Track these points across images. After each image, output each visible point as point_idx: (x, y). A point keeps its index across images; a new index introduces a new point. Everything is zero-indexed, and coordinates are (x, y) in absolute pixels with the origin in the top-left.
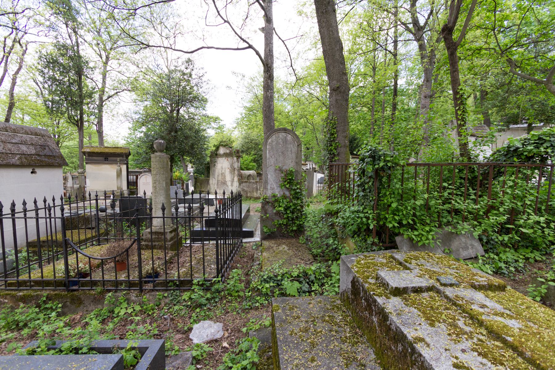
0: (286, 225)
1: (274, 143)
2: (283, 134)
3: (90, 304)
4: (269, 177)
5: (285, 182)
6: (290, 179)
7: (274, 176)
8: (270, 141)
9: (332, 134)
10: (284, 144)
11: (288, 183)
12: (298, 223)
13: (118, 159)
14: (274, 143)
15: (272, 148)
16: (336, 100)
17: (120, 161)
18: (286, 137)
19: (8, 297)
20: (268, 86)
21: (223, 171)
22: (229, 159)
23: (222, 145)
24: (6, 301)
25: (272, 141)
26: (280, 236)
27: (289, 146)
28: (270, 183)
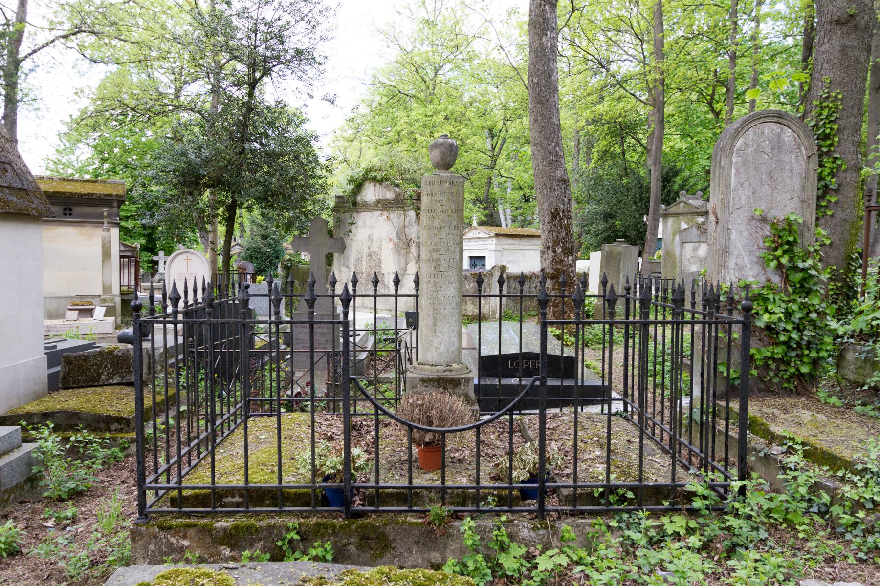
0: (784, 361)
1: (750, 150)
2: (775, 126)
3: (410, 550)
4: (734, 236)
5: (776, 249)
6: (788, 242)
7: (746, 234)
8: (739, 143)
9: (826, 137)
10: (776, 152)
11: (785, 252)
12: (814, 354)
13: (105, 211)
14: (750, 150)
15: (744, 162)
16: (844, 50)
17: (109, 216)
18: (779, 136)
19: (191, 532)
20: (546, 21)
21: (374, 248)
22: (394, 215)
23: (374, 179)
24: (186, 543)
25: (746, 145)
26: (760, 390)
27: (787, 159)
28: (736, 253)
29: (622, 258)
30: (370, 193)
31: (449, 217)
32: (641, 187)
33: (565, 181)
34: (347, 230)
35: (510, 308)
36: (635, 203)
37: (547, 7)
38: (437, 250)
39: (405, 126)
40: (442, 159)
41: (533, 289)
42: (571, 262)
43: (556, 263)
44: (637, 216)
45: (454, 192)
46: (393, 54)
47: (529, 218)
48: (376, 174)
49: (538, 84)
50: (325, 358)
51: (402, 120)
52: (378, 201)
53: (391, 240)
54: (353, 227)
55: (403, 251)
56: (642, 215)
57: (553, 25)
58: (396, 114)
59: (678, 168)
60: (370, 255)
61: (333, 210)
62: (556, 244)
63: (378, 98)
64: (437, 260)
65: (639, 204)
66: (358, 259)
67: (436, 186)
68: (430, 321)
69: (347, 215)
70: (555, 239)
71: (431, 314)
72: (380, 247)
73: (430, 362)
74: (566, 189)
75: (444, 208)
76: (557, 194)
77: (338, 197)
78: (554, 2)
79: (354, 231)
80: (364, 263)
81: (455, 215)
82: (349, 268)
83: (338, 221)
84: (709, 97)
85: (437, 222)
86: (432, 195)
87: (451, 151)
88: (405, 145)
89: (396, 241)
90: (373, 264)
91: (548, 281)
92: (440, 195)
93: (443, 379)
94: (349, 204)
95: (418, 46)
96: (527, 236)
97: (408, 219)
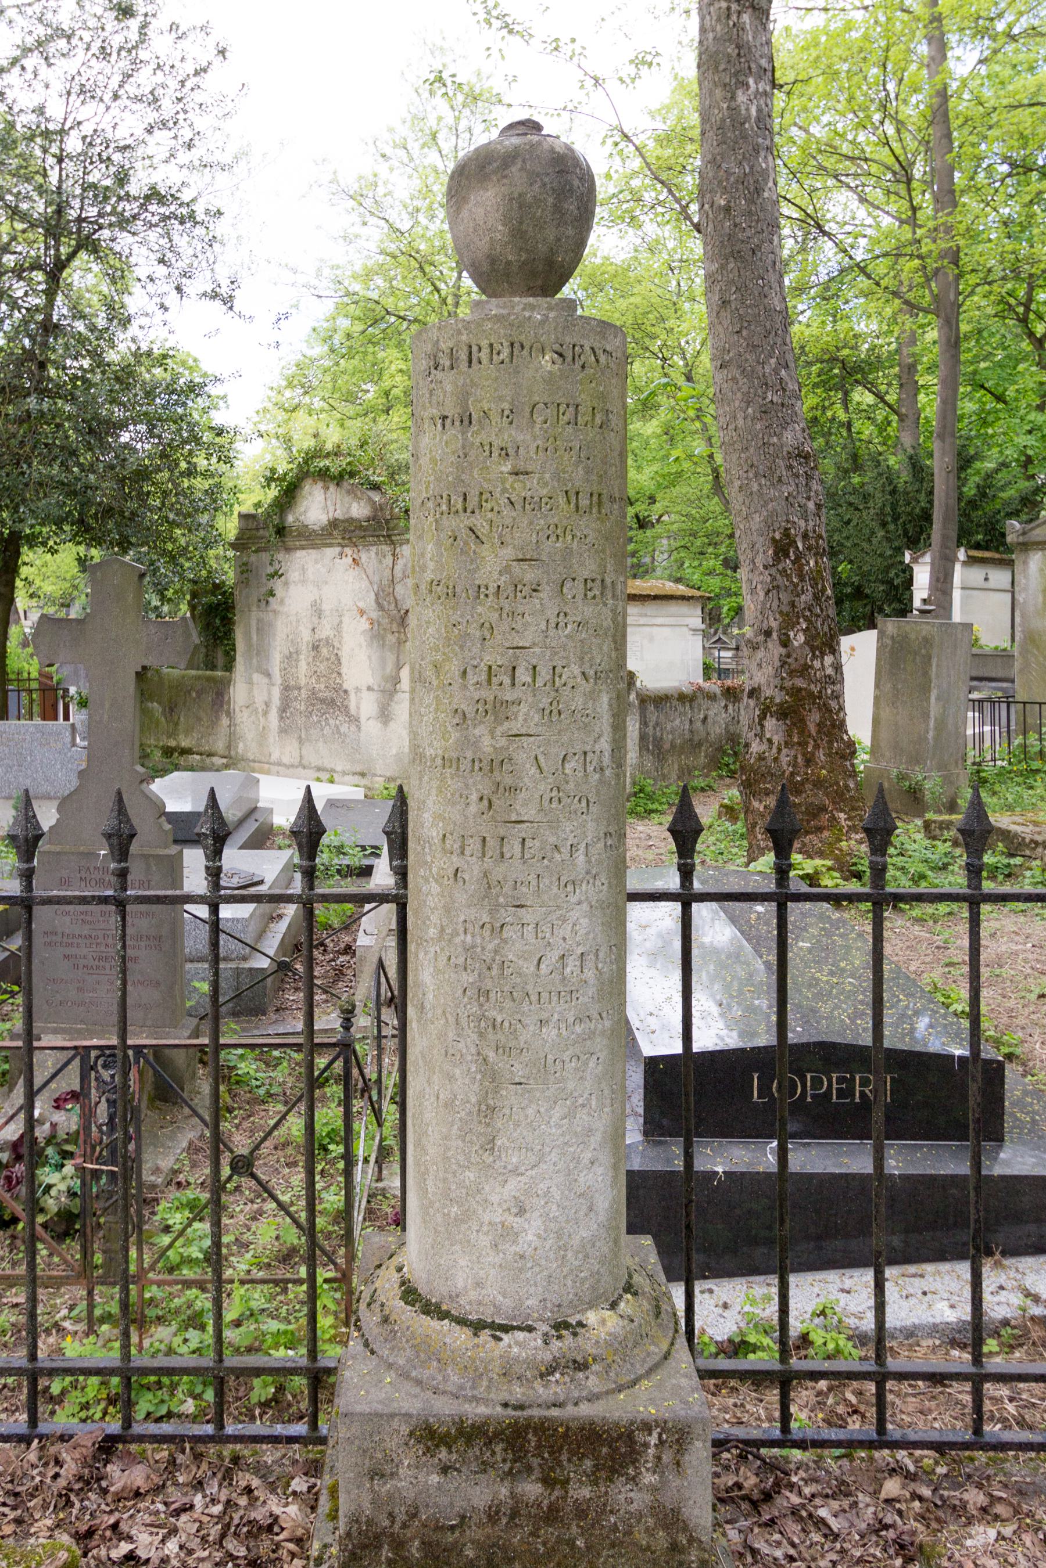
21: (326, 631)
22: (369, 556)
23: (323, 475)
29: (935, 652)
30: (316, 507)
31: (557, 532)
32: (893, 492)
33: (807, 457)
34: (263, 590)
35: (647, 775)
36: (884, 525)
37: (746, 18)
38: (498, 710)
39: (399, 378)
40: (517, 234)
41: (699, 724)
42: (829, 671)
43: (792, 673)
44: (889, 553)
45: (585, 400)
46: (373, 238)
47: (647, 560)
48: (327, 462)
49: (727, 209)
50: (77, 1062)
51: (393, 367)
52: (334, 524)
53: (362, 613)
54: (278, 585)
55: (391, 639)
56: (899, 551)
57: (764, 62)
58: (381, 355)
59: (972, 452)
60: (316, 648)
61: (234, 546)
62: (789, 621)
63: (344, 323)
64: (496, 764)
65: (892, 527)
66: (289, 657)
67: (486, 371)
68: (466, 1087)
69: (265, 556)
70: (786, 609)
71: (468, 1044)
72: (338, 627)
73: (469, 1305)
74: (809, 477)
75: (533, 487)
76: (786, 490)
77: (244, 517)
78: (764, 4)
79: (279, 592)
80: (303, 666)
81: (588, 526)
82: (268, 675)
83: (245, 570)
84: (1021, 310)
85: (492, 564)
86: (466, 420)
87: (563, 192)
88: (399, 416)
89: (374, 615)
90: (322, 667)
91: (770, 723)
92: (510, 416)
93: (542, 1428)
94: (271, 532)
95: (422, 218)
96: (656, 597)
97: (401, 562)
